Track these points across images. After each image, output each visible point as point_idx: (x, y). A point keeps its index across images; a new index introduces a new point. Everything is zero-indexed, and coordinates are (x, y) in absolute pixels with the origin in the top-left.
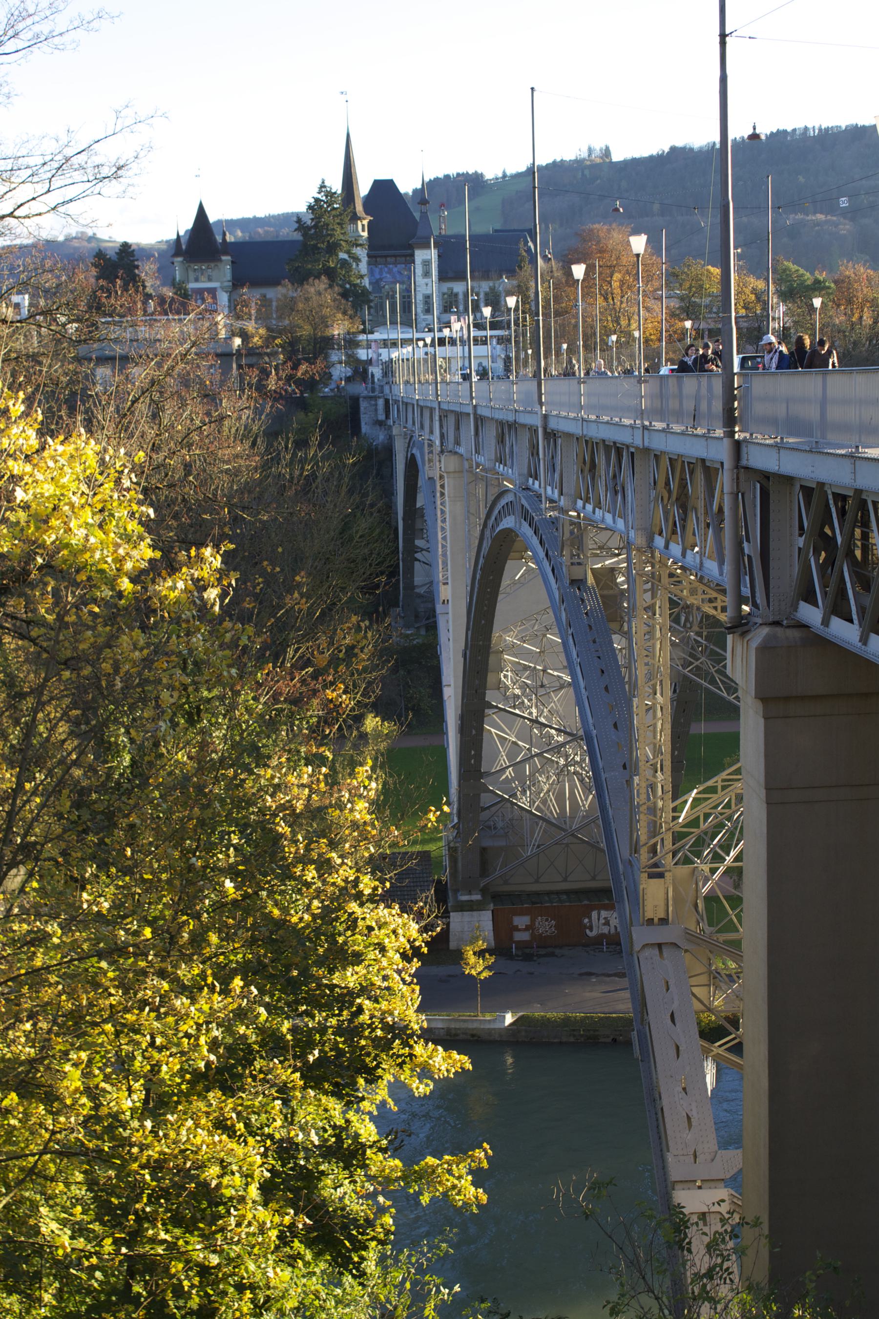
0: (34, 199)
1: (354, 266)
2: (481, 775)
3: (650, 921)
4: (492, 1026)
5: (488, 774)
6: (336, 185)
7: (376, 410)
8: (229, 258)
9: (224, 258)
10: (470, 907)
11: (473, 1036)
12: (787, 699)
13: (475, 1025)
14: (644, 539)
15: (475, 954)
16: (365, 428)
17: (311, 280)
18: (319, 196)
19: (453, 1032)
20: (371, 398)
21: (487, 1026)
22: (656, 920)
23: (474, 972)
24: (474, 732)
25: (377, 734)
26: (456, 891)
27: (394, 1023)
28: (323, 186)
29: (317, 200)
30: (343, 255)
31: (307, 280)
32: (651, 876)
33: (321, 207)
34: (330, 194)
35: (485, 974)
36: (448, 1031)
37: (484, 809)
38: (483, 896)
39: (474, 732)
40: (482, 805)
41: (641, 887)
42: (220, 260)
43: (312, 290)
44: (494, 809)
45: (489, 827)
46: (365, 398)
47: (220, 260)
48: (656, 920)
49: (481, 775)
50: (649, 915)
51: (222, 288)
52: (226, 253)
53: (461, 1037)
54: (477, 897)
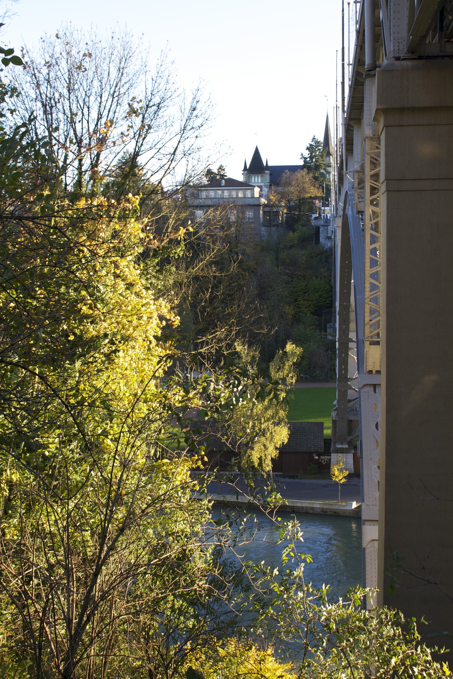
0: (179, 142)
1: (328, 175)
2: (348, 380)
3: (370, 372)
4: (345, 508)
5: (351, 379)
6: (321, 139)
7: (327, 232)
8: (269, 172)
9: (266, 172)
10: (342, 451)
11: (335, 513)
12: (402, 110)
13: (336, 507)
14: (371, 131)
15: (338, 470)
16: (322, 240)
17: (299, 170)
18: (312, 143)
19: (325, 510)
20: (325, 226)
21: (343, 508)
22: (374, 372)
23: (337, 480)
24: (343, 355)
25: (293, 354)
26: (335, 443)
27: (171, 379)
28: (314, 139)
29: (311, 145)
30: (322, 171)
31: (297, 170)
32: (372, 343)
33: (313, 148)
34: (317, 143)
35: (344, 481)
36: (322, 509)
37: (350, 401)
38: (349, 446)
39: (343, 355)
40: (348, 398)
41: (365, 350)
42: (265, 173)
43: (299, 175)
44: (355, 401)
45: (353, 410)
46: (322, 226)
47: (265, 173)
48: (374, 372)
49: (348, 380)
50: (370, 368)
51: (265, 186)
52: (267, 170)
53: (329, 513)
54: (346, 446)
